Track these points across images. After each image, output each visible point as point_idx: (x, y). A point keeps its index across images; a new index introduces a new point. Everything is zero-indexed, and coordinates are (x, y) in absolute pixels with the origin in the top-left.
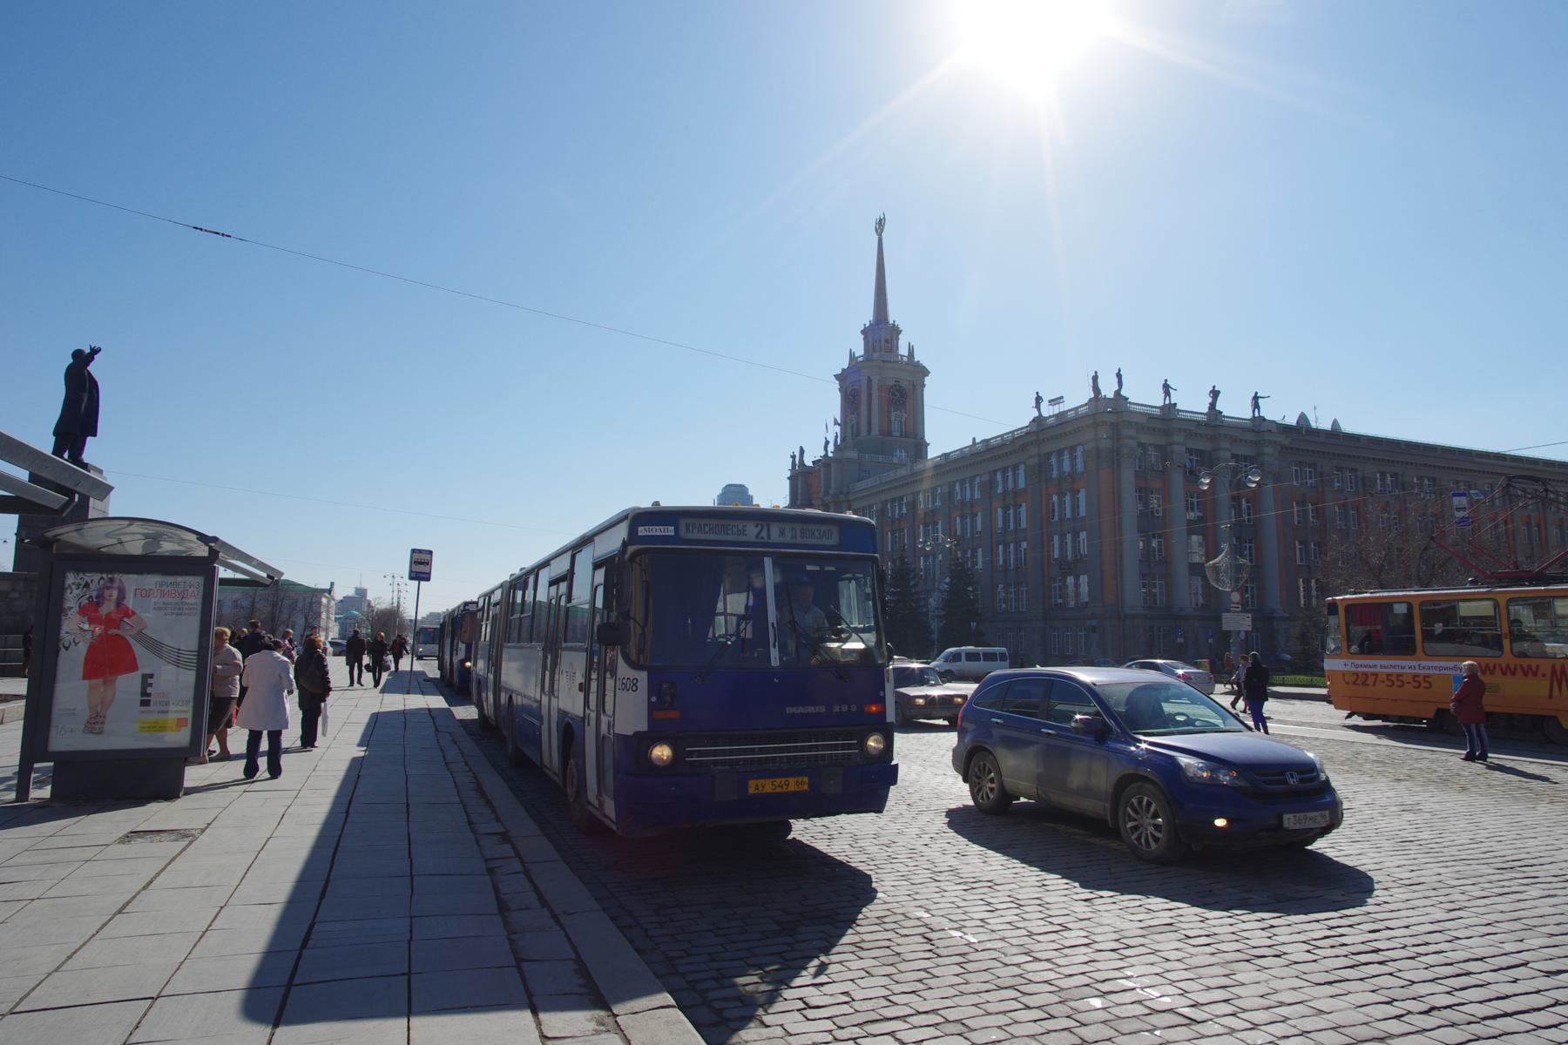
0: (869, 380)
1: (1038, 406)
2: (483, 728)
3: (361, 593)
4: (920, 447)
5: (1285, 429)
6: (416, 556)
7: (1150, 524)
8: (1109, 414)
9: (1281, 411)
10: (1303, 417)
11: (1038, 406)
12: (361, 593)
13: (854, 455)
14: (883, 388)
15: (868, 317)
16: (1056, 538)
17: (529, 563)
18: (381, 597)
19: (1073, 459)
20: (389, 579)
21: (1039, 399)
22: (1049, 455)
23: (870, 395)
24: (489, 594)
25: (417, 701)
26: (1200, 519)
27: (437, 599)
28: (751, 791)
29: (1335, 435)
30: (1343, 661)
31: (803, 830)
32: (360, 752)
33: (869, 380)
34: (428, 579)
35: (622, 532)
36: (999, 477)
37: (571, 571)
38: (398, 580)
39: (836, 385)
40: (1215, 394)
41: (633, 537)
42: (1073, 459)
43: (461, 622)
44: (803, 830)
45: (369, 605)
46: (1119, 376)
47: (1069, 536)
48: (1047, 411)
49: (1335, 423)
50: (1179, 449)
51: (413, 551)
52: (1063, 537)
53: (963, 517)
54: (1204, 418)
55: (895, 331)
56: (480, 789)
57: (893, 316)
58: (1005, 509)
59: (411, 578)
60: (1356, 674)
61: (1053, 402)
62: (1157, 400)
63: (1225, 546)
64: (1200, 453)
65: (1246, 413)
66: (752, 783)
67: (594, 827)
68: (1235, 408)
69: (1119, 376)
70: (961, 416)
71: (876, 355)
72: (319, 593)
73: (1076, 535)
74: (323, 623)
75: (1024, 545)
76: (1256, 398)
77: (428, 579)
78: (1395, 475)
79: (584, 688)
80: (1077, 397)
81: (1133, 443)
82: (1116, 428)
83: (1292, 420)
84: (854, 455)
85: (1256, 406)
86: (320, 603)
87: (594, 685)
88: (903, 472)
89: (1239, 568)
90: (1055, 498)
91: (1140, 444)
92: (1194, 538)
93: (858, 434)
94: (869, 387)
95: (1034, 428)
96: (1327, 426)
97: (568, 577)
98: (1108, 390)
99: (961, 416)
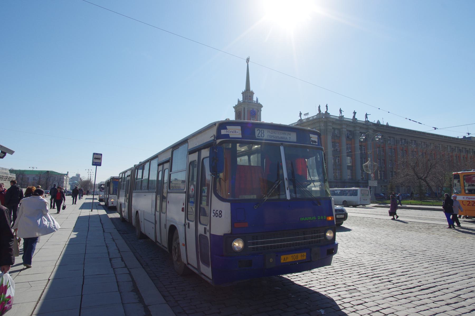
0: (244, 108)
2: (122, 219)
3: (78, 175)
5: (374, 124)
6: (96, 156)
8: (323, 119)
9: (373, 119)
10: (378, 121)
12: (78, 175)
15: (243, 89)
17: (143, 159)
18: (85, 177)
20: (87, 171)
21: (301, 114)
23: (244, 113)
25: (95, 212)
26: (351, 152)
27: (102, 176)
28: (282, 261)
29: (387, 126)
30: (462, 197)
32: (74, 235)
33: (244, 108)
34: (100, 165)
35: (214, 132)
37: (172, 158)
38: (90, 171)
40: (355, 113)
41: (219, 136)
43: (114, 184)
45: (81, 178)
46: (327, 106)
48: (303, 117)
49: (387, 123)
50: (344, 130)
51: (94, 154)
54: (351, 120)
55: (252, 93)
56: (136, 290)
57: (252, 89)
59: (93, 165)
60: (469, 202)
61: (305, 115)
62: (338, 114)
63: (369, 159)
64: (350, 131)
66: (282, 257)
67: (189, 274)
68: (361, 118)
69: (327, 106)
71: (246, 101)
72: (63, 175)
74: (64, 185)
76: (366, 115)
77: (100, 165)
80: (313, 113)
81: (331, 128)
82: (326, 123)
85: (366, 117)
86: (63, 178)
89: (374, 166)
91: (333, 128)
92: (349, 158)
94: (244, 111)
95: (299, 123)
96: (385, 124)
97: (170, 161)
98: (323, 111)
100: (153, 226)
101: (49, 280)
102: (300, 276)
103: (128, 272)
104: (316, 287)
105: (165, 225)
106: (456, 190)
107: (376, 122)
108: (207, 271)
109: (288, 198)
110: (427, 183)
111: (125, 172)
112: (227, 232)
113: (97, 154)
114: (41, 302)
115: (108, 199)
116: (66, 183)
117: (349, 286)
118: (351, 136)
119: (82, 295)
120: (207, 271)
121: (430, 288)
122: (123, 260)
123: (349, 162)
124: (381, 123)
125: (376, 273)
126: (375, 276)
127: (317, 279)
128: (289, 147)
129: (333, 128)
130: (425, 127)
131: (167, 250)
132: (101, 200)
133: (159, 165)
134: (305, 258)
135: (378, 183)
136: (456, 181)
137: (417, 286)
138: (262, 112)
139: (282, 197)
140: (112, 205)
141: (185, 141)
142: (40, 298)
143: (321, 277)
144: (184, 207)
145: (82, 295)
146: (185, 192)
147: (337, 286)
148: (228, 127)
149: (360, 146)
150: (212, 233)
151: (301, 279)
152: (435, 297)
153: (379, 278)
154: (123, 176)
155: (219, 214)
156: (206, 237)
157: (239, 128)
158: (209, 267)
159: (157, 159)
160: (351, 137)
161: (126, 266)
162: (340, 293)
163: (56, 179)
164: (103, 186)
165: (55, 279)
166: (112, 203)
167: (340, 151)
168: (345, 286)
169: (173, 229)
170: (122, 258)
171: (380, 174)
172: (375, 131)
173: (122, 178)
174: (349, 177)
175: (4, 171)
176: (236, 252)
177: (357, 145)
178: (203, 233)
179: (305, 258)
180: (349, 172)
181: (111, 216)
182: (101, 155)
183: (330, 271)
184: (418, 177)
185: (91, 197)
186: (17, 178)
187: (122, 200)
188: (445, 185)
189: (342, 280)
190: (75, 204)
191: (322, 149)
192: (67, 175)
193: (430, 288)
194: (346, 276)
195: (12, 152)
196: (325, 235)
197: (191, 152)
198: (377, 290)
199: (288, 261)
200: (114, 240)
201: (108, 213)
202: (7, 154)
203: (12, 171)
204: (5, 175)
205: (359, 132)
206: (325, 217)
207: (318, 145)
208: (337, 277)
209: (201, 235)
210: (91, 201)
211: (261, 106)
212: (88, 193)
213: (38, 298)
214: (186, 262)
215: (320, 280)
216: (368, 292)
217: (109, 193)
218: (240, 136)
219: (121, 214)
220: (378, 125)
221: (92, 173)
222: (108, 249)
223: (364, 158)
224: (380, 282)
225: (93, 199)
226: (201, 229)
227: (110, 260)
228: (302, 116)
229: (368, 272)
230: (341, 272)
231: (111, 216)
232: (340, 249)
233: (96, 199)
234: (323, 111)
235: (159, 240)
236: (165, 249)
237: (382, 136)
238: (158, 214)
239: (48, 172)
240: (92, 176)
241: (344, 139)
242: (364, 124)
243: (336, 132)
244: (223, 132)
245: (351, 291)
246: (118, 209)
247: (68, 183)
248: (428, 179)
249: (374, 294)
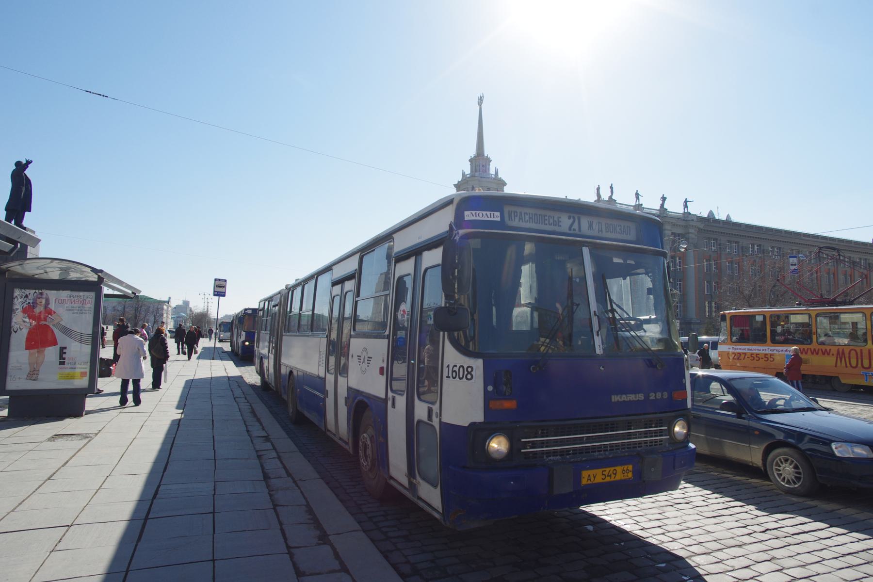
3: (186, 303)
5: (701, 219)
6: (218, 283)
9: (699, 209)
10: (711, 213)
12: (186, 303)
15: (473, 152)
17: (292, 282)
18: (197, 306)
20: (202, 296)
27: (229, 307)
28: (584, 482)
30: (728, 346)
32: (177, 415)
34: (224, 296)
40: (664, 199)
43: (248, 320)
45: (191, 310)
46: (611, 188)
51: (216, 280)
54: (657, 212)
55: (488, 160)
57: (487, 152)
62: (632, 202)
65: (680, 210)
66: (585, 474)
67: (397, 503)
68: (675, 207)
69: (611, 188)
71: (477, 174)
76: (686, 202)
77: (224, 296)
78: (759, 246)
83: (705, 215)
85: (686, 206)
86: (163, 309)
96: (723, 217)
98: (605, 196)
104: (628, 526)
108: (431, 495)
111: (270, 299)
120: (431, 495)
124: (717, 217)
141: (328, 269)
144: (385, 365)
146: (388, 337)
150: (444, 420)
151: (615, 513)
154: (266, 307)
156: (432, 426)
158: (435, 487)
163: (151, 309)
178: (425, 418)
191: (664, 255)
197: (335, 284)
205: (670, 233)
209: (419, 422)
219: (261, 372)
226: (421, 411)
236: (344, 445)
240: (210, 305)
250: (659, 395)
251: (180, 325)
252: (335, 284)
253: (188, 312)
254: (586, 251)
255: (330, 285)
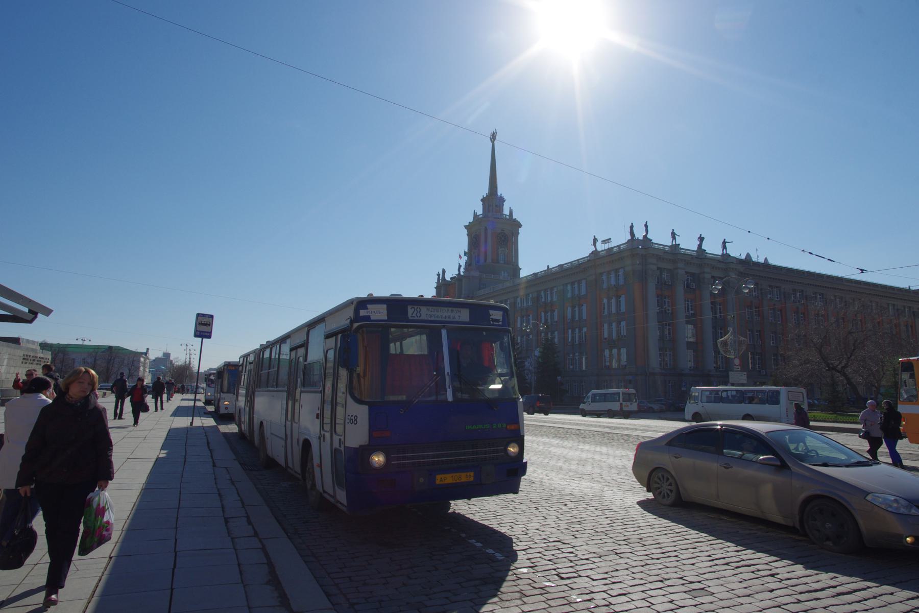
0: (486, 229)
1: (595, 244)
2: (241, 435)
3: (167, 355)
4: (517, 270)
7: (666, 318)
8: (639, 250)
9: (737, 251)
10: (748, 255)
11: (595, 244)
12: (167, 355)
13: (477, 274)
14: (493, 233)
15: (485, 191)
16: (606, 326)
17: (273, 337)
18: (179, 357)
19: (617, 277)
20: (185, 347)
21: (595, 240)
22: (601, 274)
24: (246, 356)
25: (198, 422)
26: (694, 315)
27: (214, 355)
28: (438, 482)
29: (766, 265)
31: (459, 506)
33: (486, 229)
34: (209, 337)
35: (350, 312)
36: (542, 294)
37: (307, 341)
39: (465, 232)
40: (701, 239)
41: (356, 318)
42: (617, 277)
43: (228, 374)
44: (459, 506)
46: (646, 226)
47: (577, 330)
48: (600, 247)
49: (766, 259)
51: (198, 315)
52: (610, 325)
53: (546, 312)
55: (502, 200)
56: (274, 581)
57: (501, 191)
58: (573, 307)
59: (196, 336)
61: (604, 242)
62: (667, 241)
63: (731, 329)
64: (693, 275)
65: (719, 251)
66: (438, 477)
67: (326, 506)
68: (713, 248)
69: (646, 226)
70: (539, 252)
72: (138, 355)
73: (619, 323)
75: (585, 330)
76: (724, 243)
77: (209, 337)
79: (320, 416)
80: (620, 238)
81: (655, 267)
84: (477, 274)
85: (724, 247)
86: (139, 361)
87: (327, 414)
88: (508, 284)
90: (605, 301)
91: (658, 268)
92: (690, 326)
93: (478, 262)
96: (762, 260)
97: (305, 345)
99: (539, 252)
100: (283, 443)
101: (111, 558)
102: (594, 560)
103: (260, 546)
105: (298, 440)
106: (906, 392)
107: (743, 257)
109: (450, 398)
110: (848, 379)
112: (363, 444)
113: (204, 315)
114: (94, 599)
115: (219, 401)
116: (144, 370)
117: (691, 582)
118: (695, 283)
119: (172, 589)
120: (342, 496)
121: (855, 591)
122: (249, 523)
123: (690, 335)
124: (754, 259)
125: (744, 557)
126: (743, 563)
127: (627, 566)
128: (457, 331)
129: (658, 268)
130: (842, 265)
131: (300, 477)
132: (208, 402)
133: (291, 350)
134: (472, 479)
135: (748, 377)
136: (905, 376)
137: (829, 588)
138: (520, 236)
139: (441, 398)
140: (226, 412)
142: (94, 592)
143: (634, 564)
145: (172, 589)
147: (667, 583)
148: (369, 306)
149: (712, 303)
152: (866, 610)
153: (752, 568)
155: (354, 421)
157: (385, 306)
159: (322, 326)
160: (694, 286)
161: (256, 534)
162: (672, 597)
164: (212, 377)
165: (119, 556)
166: (226, 408)
167: (672, 313)
168: (682, 582)
169: (307, 444)
170: (248, 517)
171: (753, 358)
172: (741, 274)
173: (242, 365)
174: (691, 364)
175: (31, 346)
176: (376, 469)
177: (707, 302)
179: (472, 479)
180: (690, 354)
181: (224, 429)
182: (212, 317)
183: (653, 551)
184: (828, 366)
185: (192, 396)
186: (54, 359)
187: (242, 402)
188: (884, 383)
189: (676, 570)
190: (162, 409)
191: (508, 331)
192: (146, 354)
193: (855, 591)
194: (684, 562)
195: (47, 312)
196: (506, 450)
197: (328, 336)
198: (747, 592)
199: (447, 482)
200: (233, 483)
201: (218, 424)
202: (39, 315)
203: (44, 346)
204: (32, 354)
206: (505, 425)
207: (502, 325)
208: (668, 565)
210: (191, 403)
211: (519, 225)
212: (182, 390)
213: (90, 592)
214: (321, 490)
215: (634, 570)
216: (729, 595)
217: (222, 391)
218: (386, 318)
219: (239, 426)
220: (747, 262)
221: (192, 352)
222: (221, 501)
223: (720, 327)
224: (753, 576)
225: (195, 400)
227: (226, 521)
228: (599, 244)
229: (729, 554)
230: (675, 554)
231: (224, 429)
232: (529, 469)
233: (199, 400)
234: (639, 234)
235: (290, 465)
237: (756, 284)
238: (289, 423)
239: (110, 348)
240: (193, 356)
241: (680, 290)
242: (719, 261)
243: (665, 275)
244: (363, 313)
245: (694, 593)
246: (237, 418)
247: (147, 370)
248: (849, 370)
249: (741, 600)
250: (499, 426)
251: (159, 378)
252: (328, 336)
253: (169, 365)
254: (444, 333)
255: (323, 337)
